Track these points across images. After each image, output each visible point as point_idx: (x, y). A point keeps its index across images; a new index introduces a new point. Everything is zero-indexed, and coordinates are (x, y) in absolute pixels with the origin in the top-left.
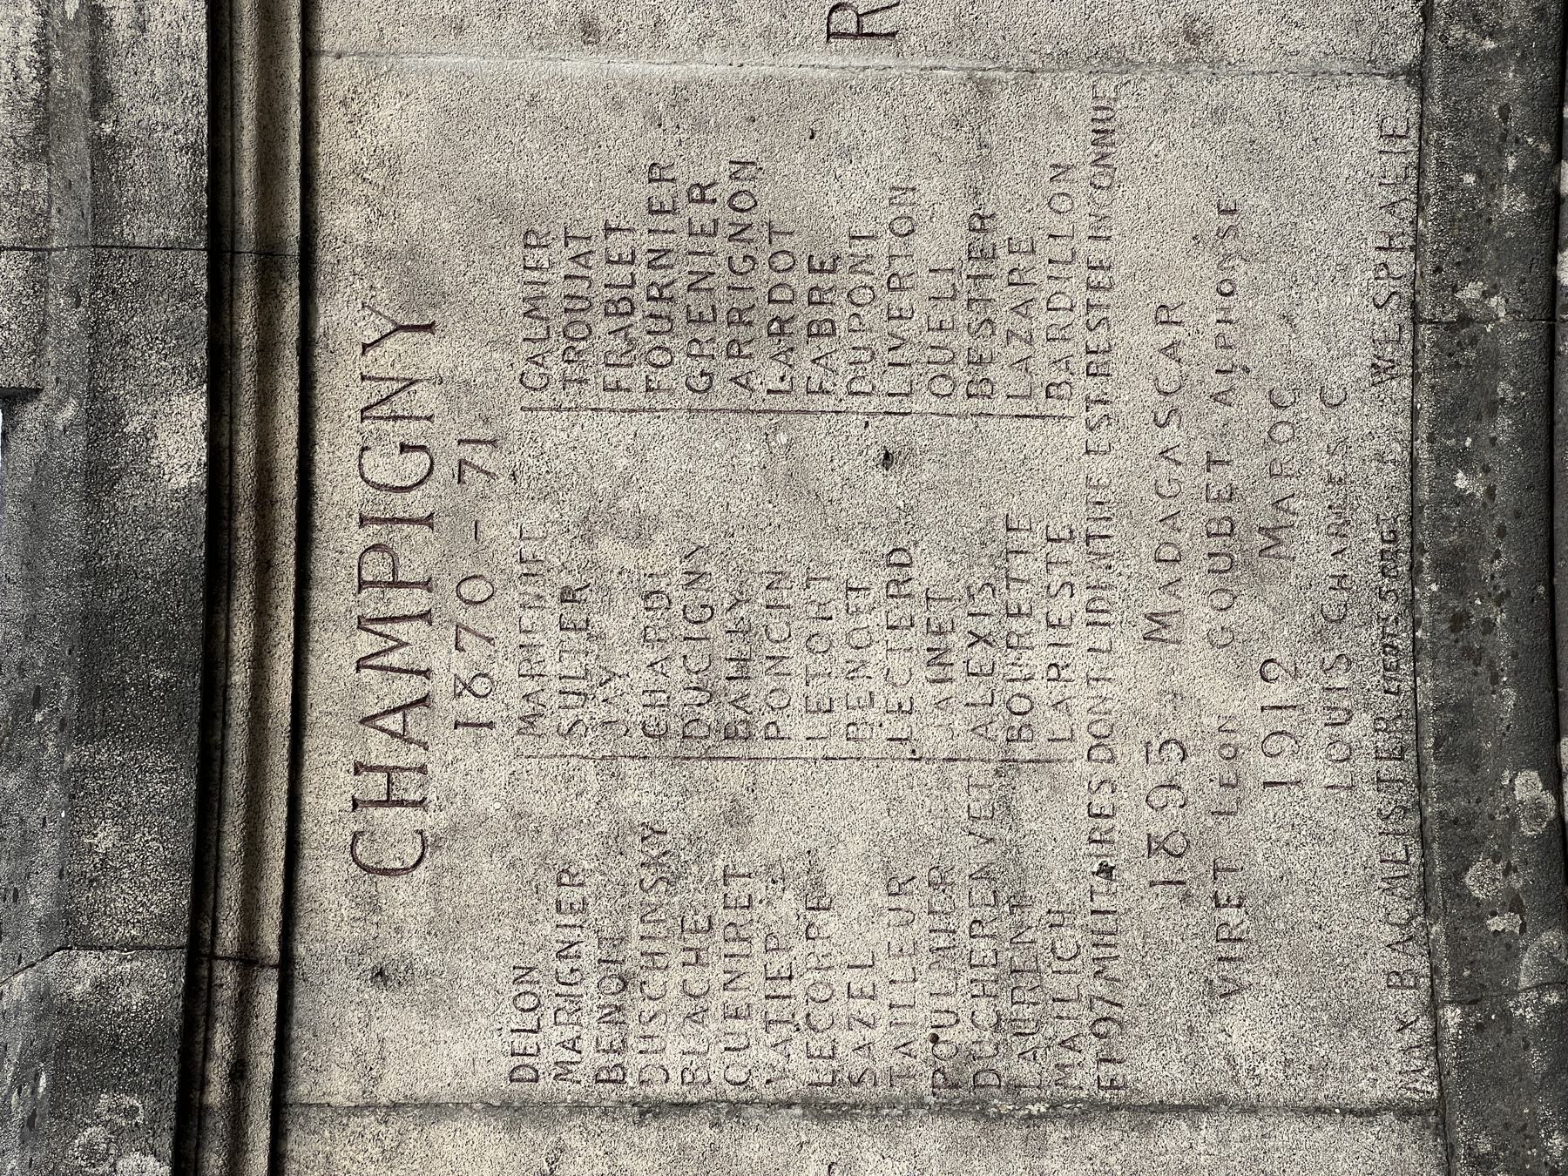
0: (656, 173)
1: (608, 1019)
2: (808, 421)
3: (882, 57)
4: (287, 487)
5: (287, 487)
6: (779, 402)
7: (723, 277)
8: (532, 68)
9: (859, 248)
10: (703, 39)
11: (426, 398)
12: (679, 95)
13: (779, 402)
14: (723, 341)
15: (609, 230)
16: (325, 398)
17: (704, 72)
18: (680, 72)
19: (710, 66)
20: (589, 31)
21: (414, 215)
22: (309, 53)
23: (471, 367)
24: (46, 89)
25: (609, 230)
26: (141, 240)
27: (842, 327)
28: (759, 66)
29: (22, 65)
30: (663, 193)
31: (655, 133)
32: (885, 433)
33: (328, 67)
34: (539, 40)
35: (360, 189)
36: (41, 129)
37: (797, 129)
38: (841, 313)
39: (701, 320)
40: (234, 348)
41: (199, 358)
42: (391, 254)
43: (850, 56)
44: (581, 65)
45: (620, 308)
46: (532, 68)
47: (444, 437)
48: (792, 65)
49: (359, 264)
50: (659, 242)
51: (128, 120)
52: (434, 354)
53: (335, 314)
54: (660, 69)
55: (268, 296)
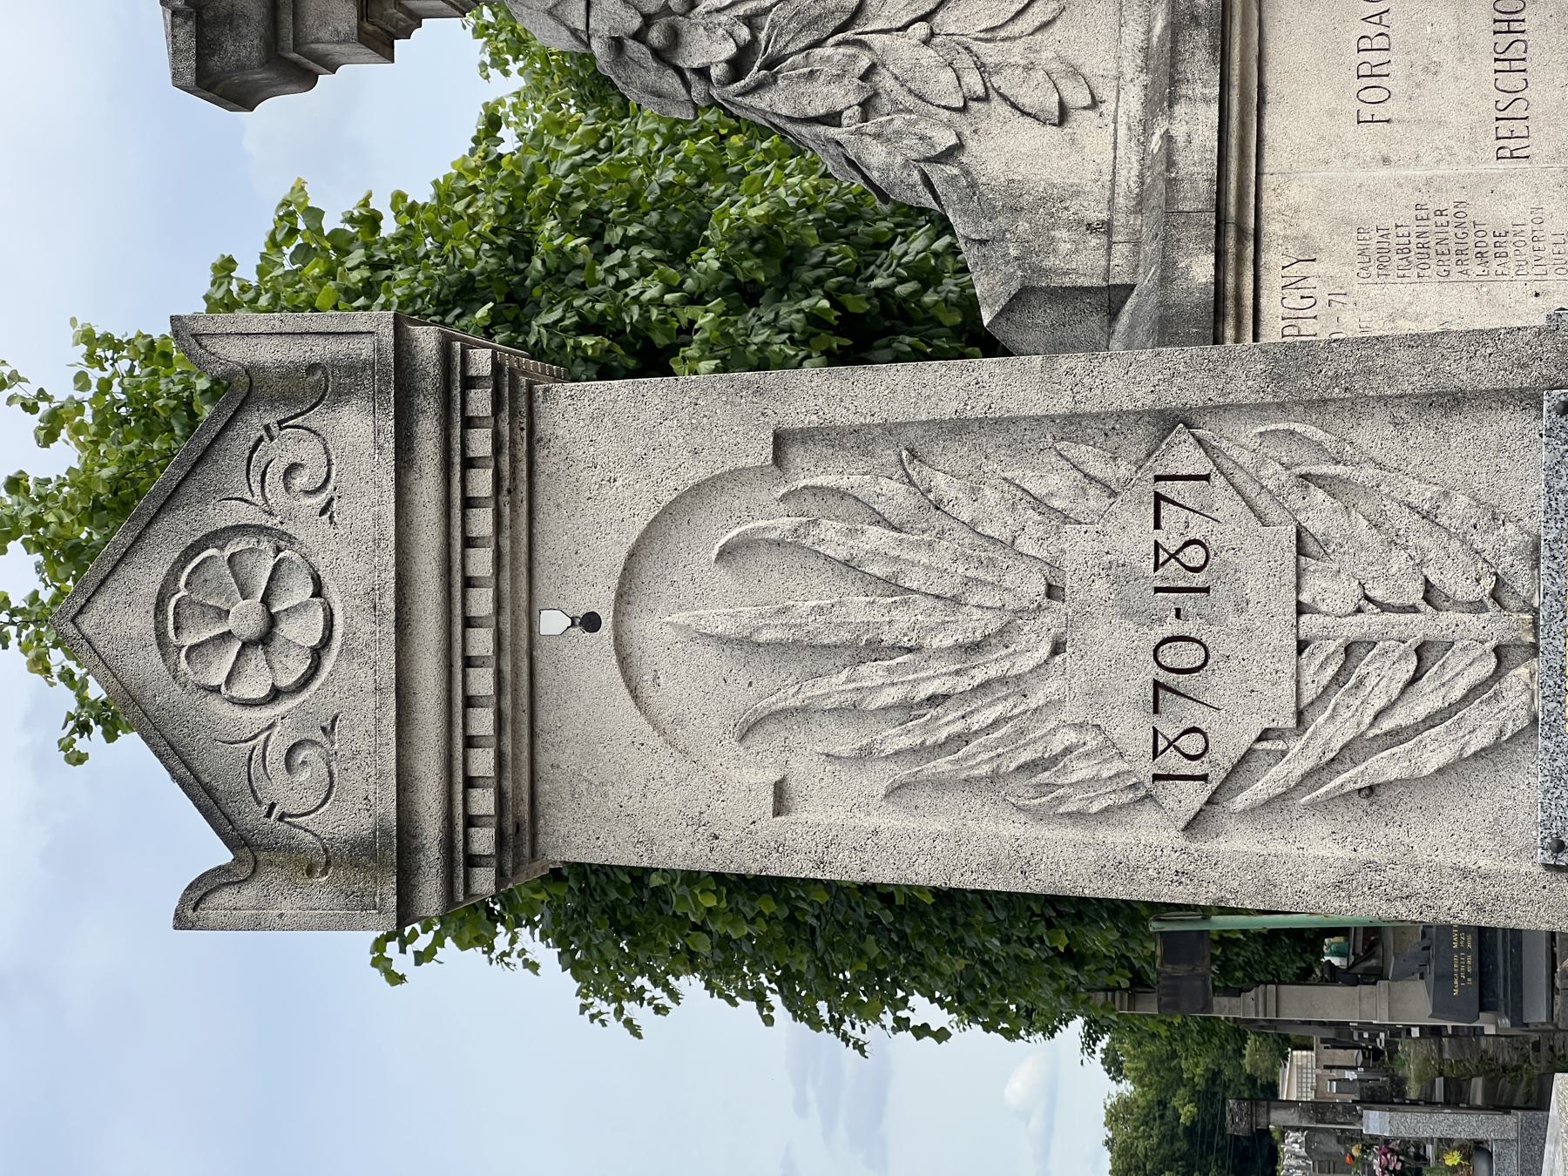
0: (1418, 207)
1: (1349, 778)
2: (1496, 284)
3: (1523, 164)
4: (1248, 301)
5: (1248, 301)
6: (1482, 278)
7: (1453, 239)
8: (1360, 175)
9: (1518, 229)
10: (1438, 161)
11: (1312, 281)
12: (1429, 182)
13: (1482, 278)
14: (1453, 260)
15: (1397, 226)
16: (1264, 283)
17: (1440, 173)
18: (1429, 173)
19: (1443, 170)
20: (1386, 161)
21: (1306, 225)
22: (1259, 174)
23: (1335, 271)
24: (1142, 191)
25: (1397, 226)
26: (1187, 209)
27: (1511, 254)
28: (1465, 169)
29: (1131, 183)
30: (1423, 214)
31: (1417, 194)
32: (1536, 287)
33: (1266, 178)
34: (1364, 165)
35: (1281, 217)
36: (1139, 203)
37: (1485, 189)
38: (1511, 249)
39: (1443, 254)
40: (1226, 252)
41: (1211, 244)
42: (1296, 238)
43: (1510, 164)
44: (1383, 172)
45: (1404, 251)
46: (1360, 175)
47: (1322, 296)
48: (1480, 168)
49: (1280, 242)
50: (1420, 229)
51: (1182, 173)
52: (1314, 268)
53: (1270, 257)
54: (1420, 173)
55: (1239, 275)
